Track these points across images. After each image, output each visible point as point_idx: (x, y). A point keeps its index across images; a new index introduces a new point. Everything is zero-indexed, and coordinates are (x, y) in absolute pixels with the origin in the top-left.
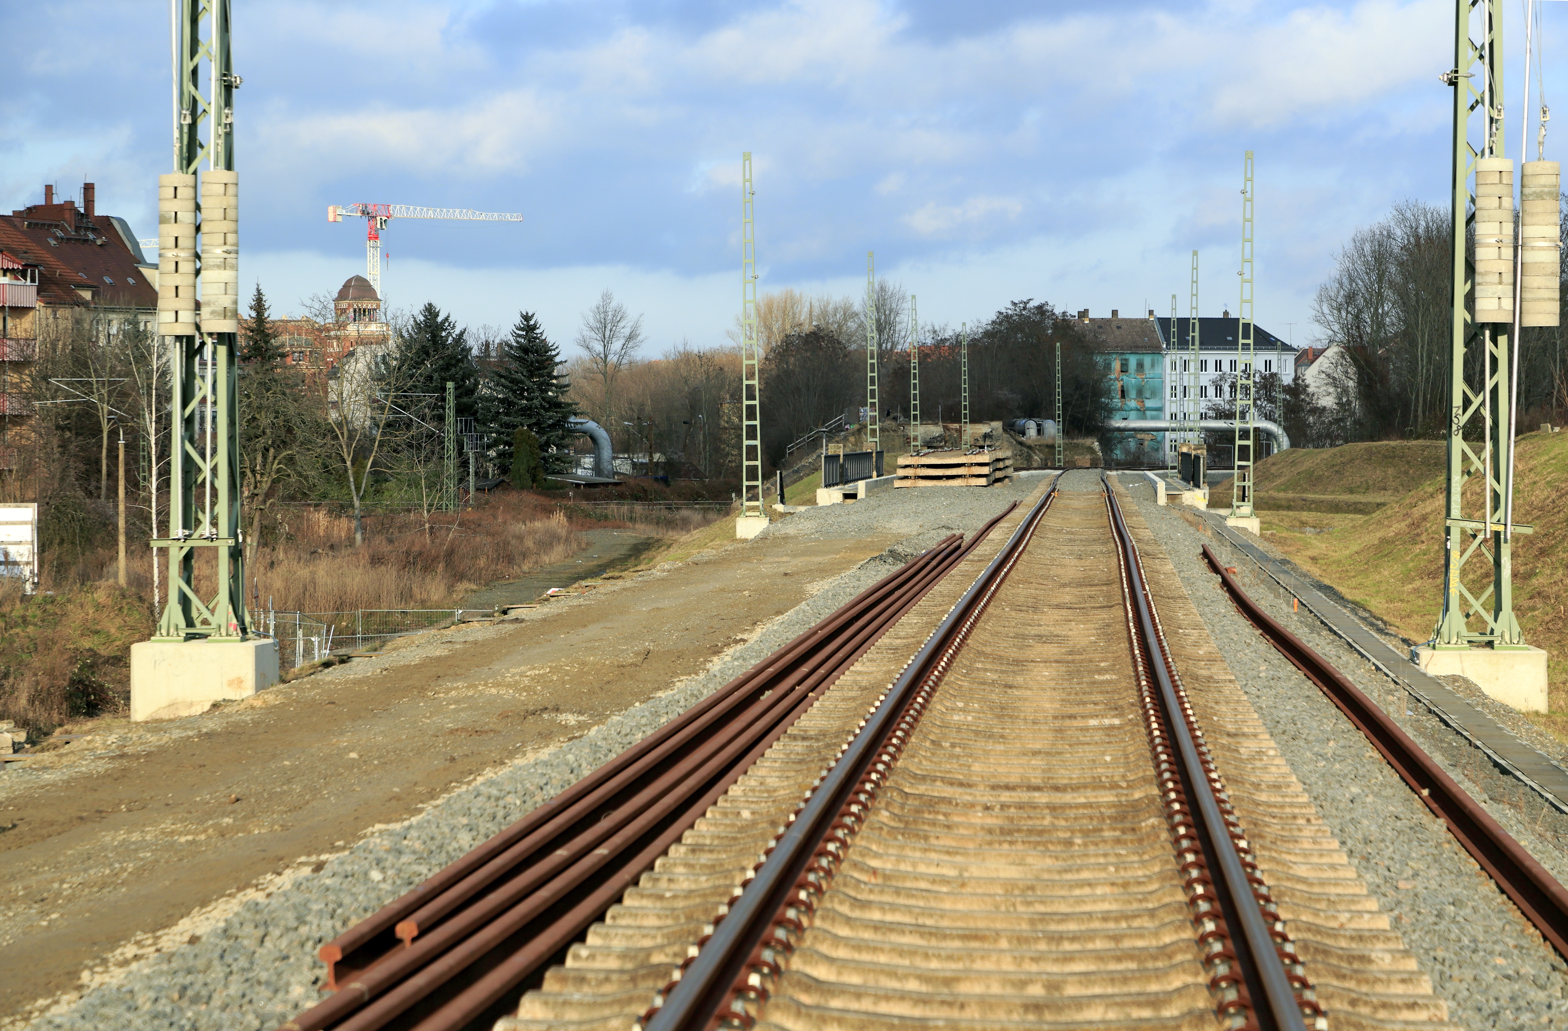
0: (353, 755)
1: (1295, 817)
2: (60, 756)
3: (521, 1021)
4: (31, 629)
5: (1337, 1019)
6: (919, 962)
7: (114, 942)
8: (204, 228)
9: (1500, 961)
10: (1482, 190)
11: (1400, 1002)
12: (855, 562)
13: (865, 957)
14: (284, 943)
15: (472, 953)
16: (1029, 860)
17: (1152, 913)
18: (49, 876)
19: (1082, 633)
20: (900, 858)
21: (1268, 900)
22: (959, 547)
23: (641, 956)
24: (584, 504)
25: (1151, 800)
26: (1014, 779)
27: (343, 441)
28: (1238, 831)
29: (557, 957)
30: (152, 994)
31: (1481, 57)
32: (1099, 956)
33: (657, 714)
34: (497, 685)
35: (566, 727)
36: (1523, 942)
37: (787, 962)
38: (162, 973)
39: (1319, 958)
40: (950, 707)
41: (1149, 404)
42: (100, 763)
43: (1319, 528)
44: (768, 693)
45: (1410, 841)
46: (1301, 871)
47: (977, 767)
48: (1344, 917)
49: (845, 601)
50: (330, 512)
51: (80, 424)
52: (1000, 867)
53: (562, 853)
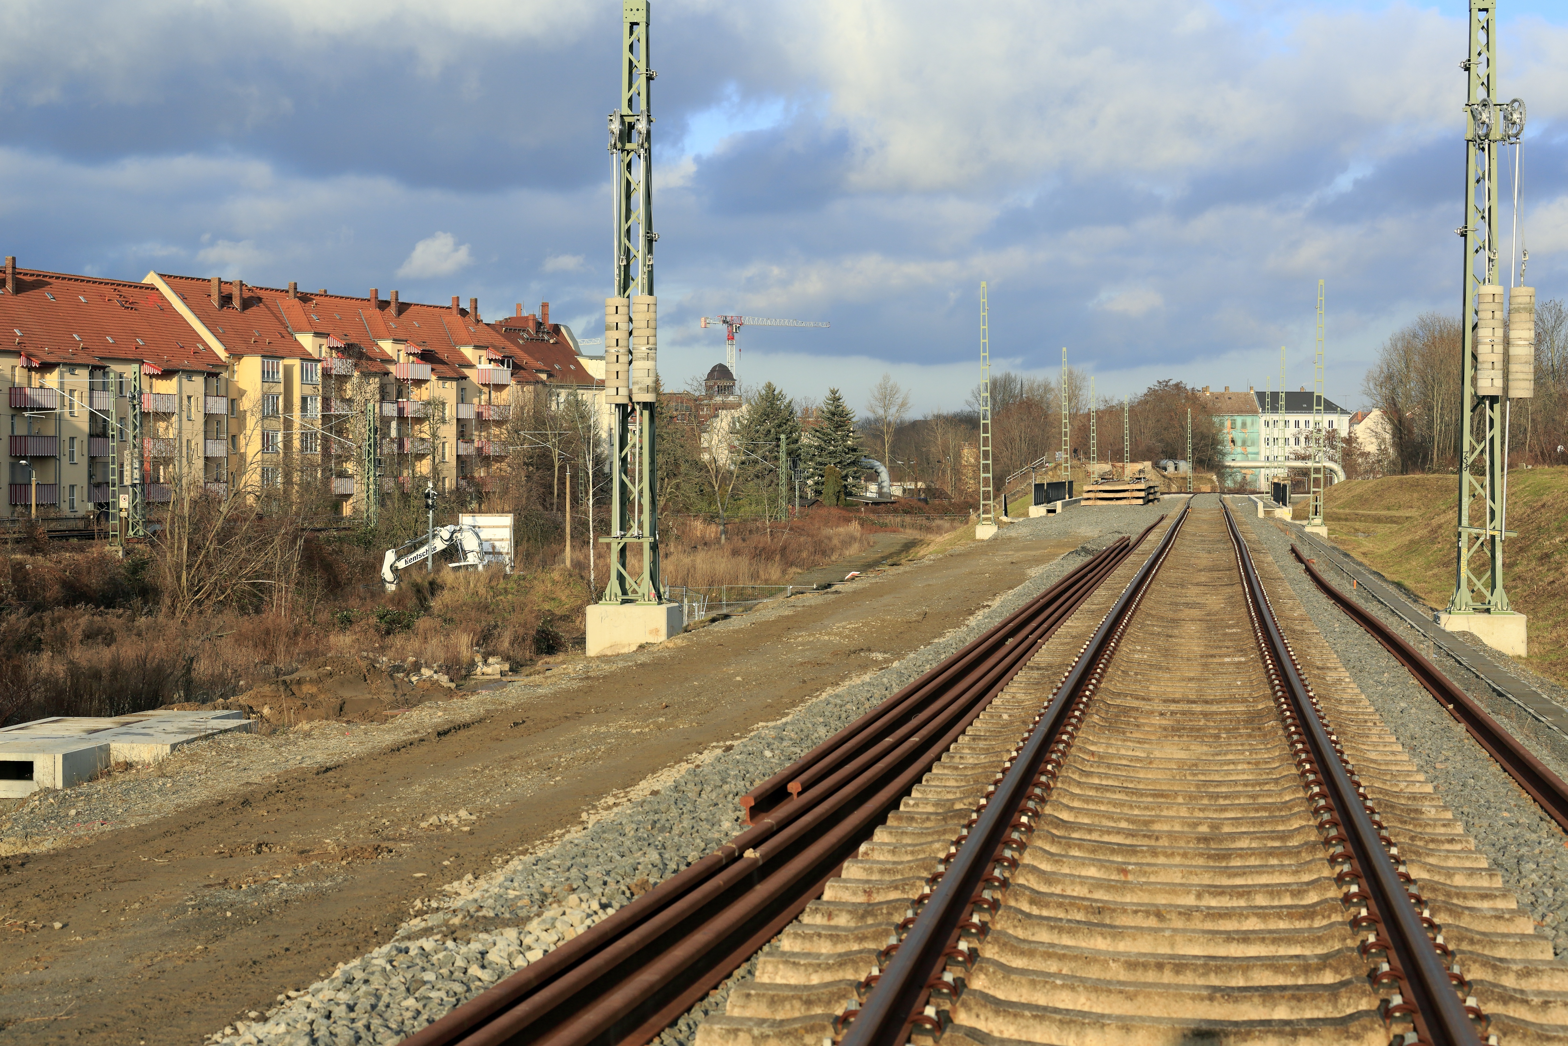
0: (739, 678)
1: (1366, 721)
2: (546, 678)
3: (876, 844)
4: (510, 597)
5: (1402, 848)
6: (1126, 810)
7: (599, 796)
8: (635, 333)
9: (1506, 814)
10: (1482, 307)
11: (1443, 838)
12: (1058, 555)
13: (1091, 807)
14: (714, 795)
15: (839, 802)
16: (1192, 747)
17: (1276, 781)
18: (551, 753)
19: (1215, 601)
20: (1109, 745)
21: (1352, 773)
22: (1128, 545)
23: (948, 804)
24: (872, 516)
25: (1270, 709)
26: (1178, 696)
27: (713, 473)
28: (1330, 729)
29: (894, 804)
30: (634, 826)
31: (1483, 217)
32: (1243, 808)
33: (938, 653)
34: (829, 634)
35: (876, 661)
36: (1520, 803)
37: (1042, 809)
38: (639, 813)
39: (1388, 810)
40: (1132, 650)
41: (1250, 449)
42: (574, 682)
43: (1367, 534)
44: (1010, 640)
45: (1442, 738)
46: (1373, 756)
47: (1152, 688)
48: (1403, 785)
49: (1055, 581)
50: (705, 520)
51: (540, 461)
52: (1174, 751)
53: (889, 740)
